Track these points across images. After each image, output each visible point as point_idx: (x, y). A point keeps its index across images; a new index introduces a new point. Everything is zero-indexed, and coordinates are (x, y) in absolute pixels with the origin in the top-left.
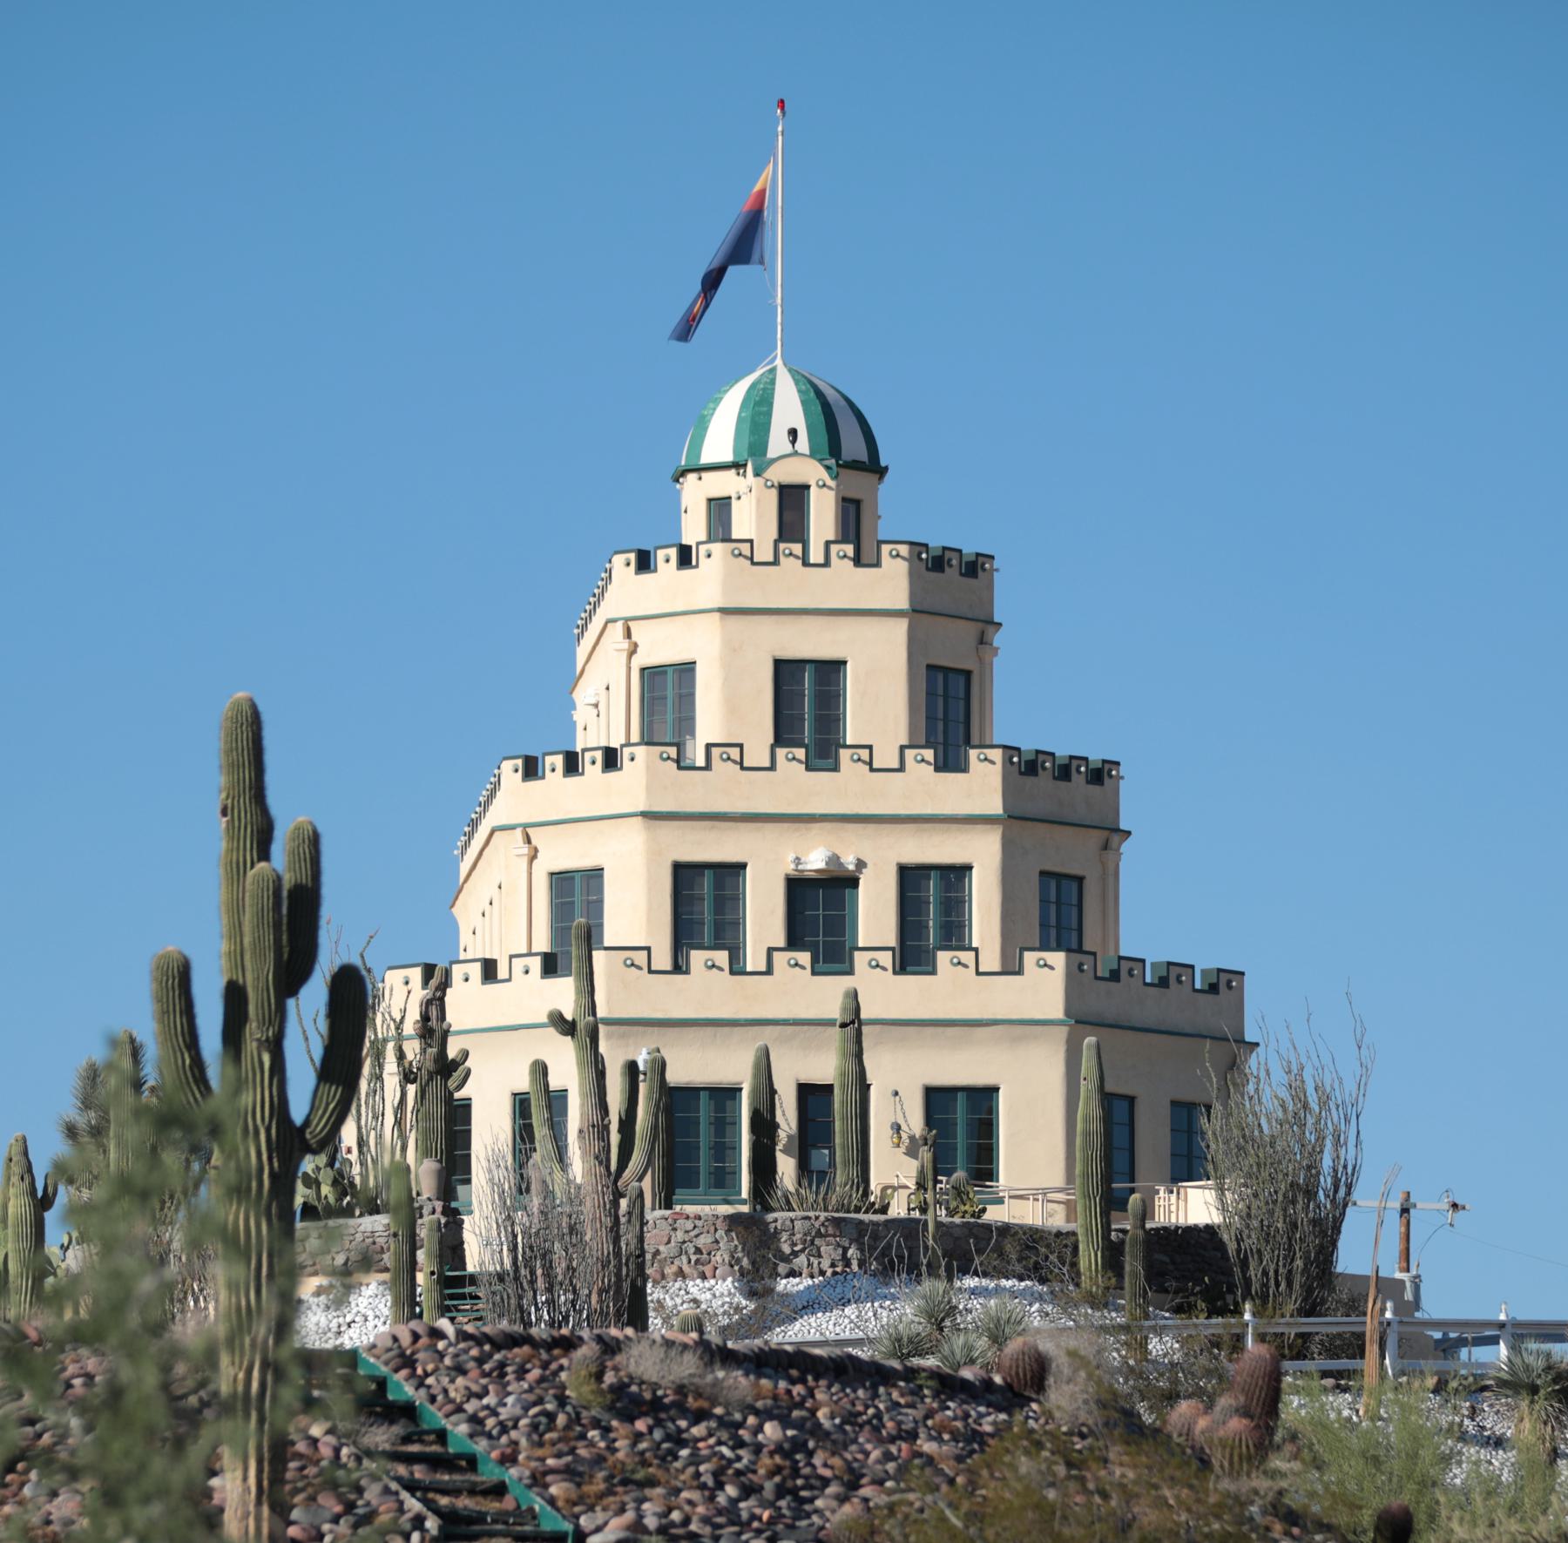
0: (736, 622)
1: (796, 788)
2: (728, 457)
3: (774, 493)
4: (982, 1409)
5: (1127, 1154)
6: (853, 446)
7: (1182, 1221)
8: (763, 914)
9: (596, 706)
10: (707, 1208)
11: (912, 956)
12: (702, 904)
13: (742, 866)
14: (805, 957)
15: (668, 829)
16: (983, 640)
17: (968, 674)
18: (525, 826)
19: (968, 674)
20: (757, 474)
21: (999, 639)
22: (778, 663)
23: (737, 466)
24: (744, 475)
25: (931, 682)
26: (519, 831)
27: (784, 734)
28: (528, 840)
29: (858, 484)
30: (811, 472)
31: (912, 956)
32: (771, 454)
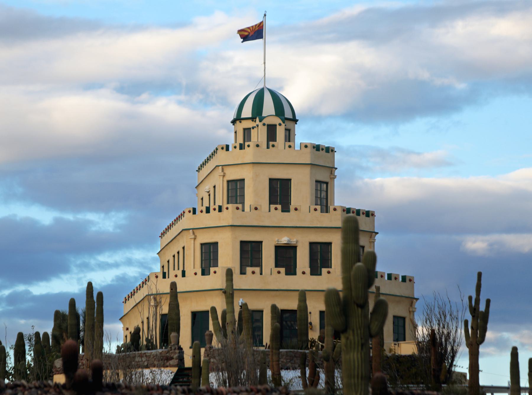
0: (258, 168)
1: (277, 216)
2: (250, 116)
3: (266, 127)
4: (32, 355)
5: (135, 304)
6: (288, 114)
7: (399, 353)
8: (268, 256)
9: (208, 192)
10: (296, 350)
11: (315, 271)
12: (250, 253)
13: (261, 242)
14: (283, 270)
15: (238, 231)
16: (332, 173)
17: (327, 183)
18: (193, 229)
19: (327, 183)
20: (260, 121)
21: (336, 173)
22: (271, 180)
23: (253, 119)
24: (255, 122)
25: (316, 186)
26: (191, 231)
27: (272, 201)
28: (194, 234)
29: (289, 124)
30: (277, 121)
31: (315, 271)
32: (264, 115)
